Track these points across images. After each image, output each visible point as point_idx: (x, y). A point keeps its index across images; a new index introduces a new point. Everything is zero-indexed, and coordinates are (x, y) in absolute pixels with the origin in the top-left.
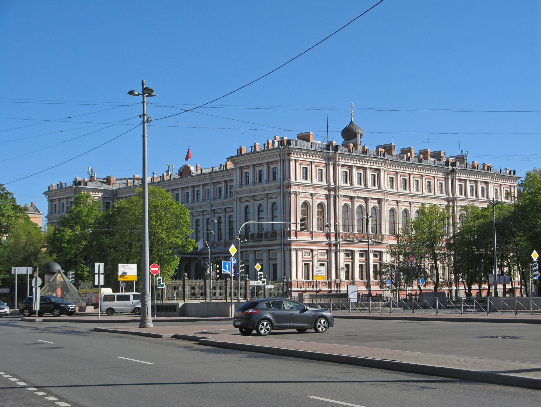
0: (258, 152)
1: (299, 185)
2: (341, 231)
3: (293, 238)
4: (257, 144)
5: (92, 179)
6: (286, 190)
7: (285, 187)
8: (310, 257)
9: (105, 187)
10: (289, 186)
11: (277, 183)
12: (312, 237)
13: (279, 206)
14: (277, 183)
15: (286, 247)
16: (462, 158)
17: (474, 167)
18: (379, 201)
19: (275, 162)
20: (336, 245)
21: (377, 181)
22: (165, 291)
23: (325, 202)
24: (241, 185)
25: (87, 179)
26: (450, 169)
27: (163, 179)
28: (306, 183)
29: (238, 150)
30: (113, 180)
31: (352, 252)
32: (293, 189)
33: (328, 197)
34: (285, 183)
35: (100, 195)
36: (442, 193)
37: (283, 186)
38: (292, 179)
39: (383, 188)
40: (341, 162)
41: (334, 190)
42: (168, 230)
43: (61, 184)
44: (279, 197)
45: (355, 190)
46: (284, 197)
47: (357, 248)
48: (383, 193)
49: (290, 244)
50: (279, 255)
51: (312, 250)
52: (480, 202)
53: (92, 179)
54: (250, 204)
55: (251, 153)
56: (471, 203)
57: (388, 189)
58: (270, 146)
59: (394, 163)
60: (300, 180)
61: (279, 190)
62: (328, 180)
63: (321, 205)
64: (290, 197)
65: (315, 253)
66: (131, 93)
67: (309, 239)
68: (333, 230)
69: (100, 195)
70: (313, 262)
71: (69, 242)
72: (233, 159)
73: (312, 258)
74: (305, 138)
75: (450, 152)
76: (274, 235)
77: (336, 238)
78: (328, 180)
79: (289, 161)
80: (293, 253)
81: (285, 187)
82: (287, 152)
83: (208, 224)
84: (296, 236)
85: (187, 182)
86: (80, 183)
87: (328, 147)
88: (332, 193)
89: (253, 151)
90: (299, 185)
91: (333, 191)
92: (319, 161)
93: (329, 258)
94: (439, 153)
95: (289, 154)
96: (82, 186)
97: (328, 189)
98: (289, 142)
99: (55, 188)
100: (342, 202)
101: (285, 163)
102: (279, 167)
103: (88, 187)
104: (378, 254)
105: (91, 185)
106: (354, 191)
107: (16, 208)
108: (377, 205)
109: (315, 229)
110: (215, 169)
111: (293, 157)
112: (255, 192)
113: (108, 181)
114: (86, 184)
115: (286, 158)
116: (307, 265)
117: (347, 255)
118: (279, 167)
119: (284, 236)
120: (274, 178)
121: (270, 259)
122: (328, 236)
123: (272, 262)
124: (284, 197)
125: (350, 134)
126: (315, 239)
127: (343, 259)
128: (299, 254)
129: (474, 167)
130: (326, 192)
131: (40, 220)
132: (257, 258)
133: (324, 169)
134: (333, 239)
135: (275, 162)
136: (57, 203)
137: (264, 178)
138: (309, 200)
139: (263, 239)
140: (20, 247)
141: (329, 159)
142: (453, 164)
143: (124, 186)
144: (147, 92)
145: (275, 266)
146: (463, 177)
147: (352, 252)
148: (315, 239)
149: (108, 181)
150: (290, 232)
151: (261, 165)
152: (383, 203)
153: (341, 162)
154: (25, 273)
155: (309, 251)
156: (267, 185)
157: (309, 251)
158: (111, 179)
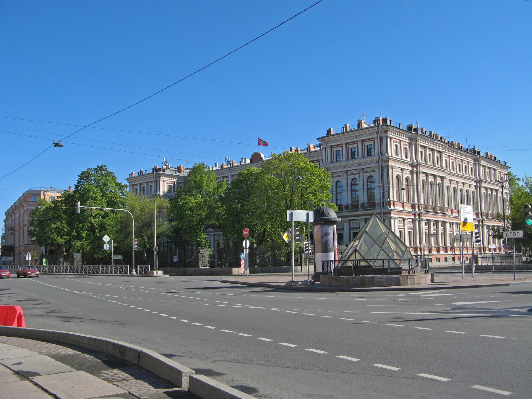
0: (349, 132)
3: (392, 207)
4: (348, 125)
6: (384, 164)
7: (383, 161)
8: (402, 225)
12: (403, 207)
15: (385, 215)
20: (419, 215)
23: (410, 176)
27: (233, 165)
29: (343, 128)
30: (183, 169)
32: (391, 163)
33: (412, 172)
34: (384, 157)
35: (175, 180)
37: (381, 161)
43: (141, 172)
44: (377, 170)
46: (382, 170)
51: (404, 219)
53: (168, 168)
61: (377, 164)
62: (411, 158)
63: (407, 179)
64: (388, 170)
65: (406, 222)
67: (402, 209)
69: (175, 180)
70: (404, 229)
71: (192, 210)
72: (324, 139)
73: (404, 226)
76: (372, 204)
77: (419, 208)
78: (411, 158)
79: (387, 137)
81: (383, 161)
82: (385, 130)
84: (394, 206)
86: (159, 169)
90: (395, 160)
93: (414, 226)
95: (160, 177)
96: (161, 172)
101: (382, 140)
103: (165, 173)
105: (167, 172)
109: (405, 201)
111: (162, 179)
112: (349, 167)
114: (164, 171)
115: (383, 135)
119: (383, 206)
121: (350, 228)
122: (413, 207)
124: (382, 170)
127: (424, 227)
132: (351, 227)
139: (359, 210)
149: (179, 169)
150: (389, 202)
153: (421, 142)
154: (304, 220)
155: (402, 219)
156: (363, 160)
157: (402, 219)
158: (182, 168)
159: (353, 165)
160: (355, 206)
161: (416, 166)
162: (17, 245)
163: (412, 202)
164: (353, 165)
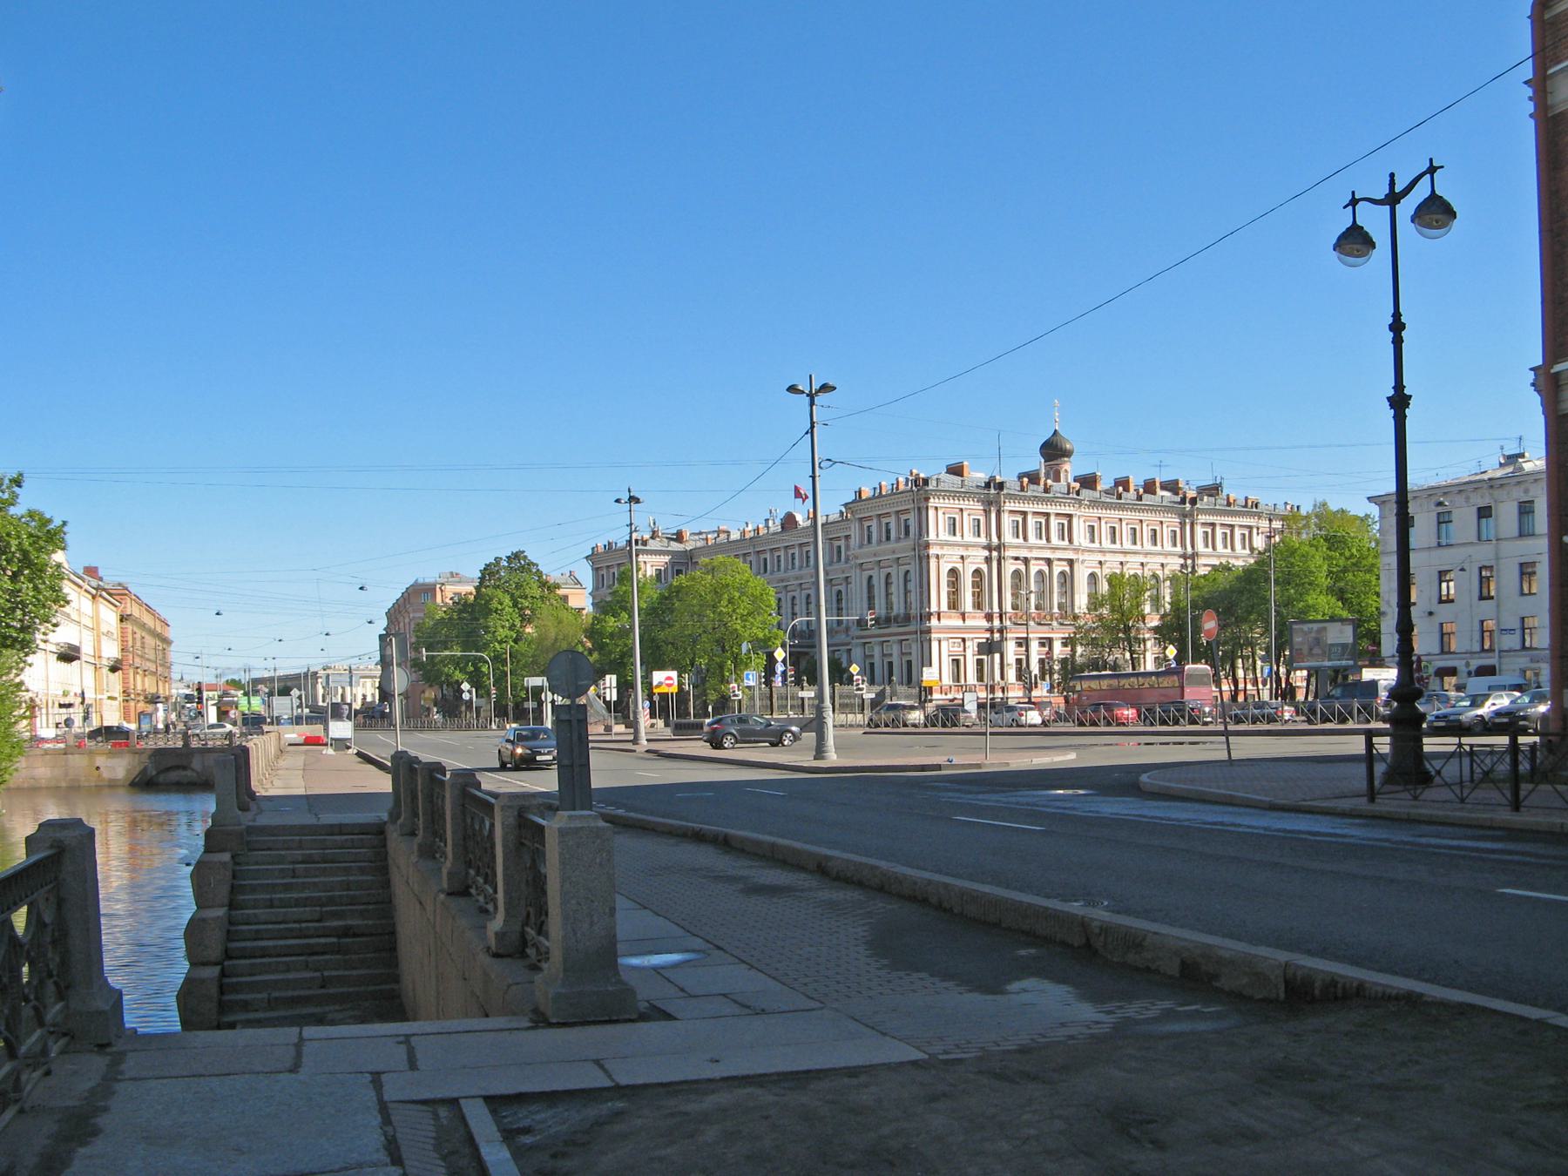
1: (942, 545)
2: (1009, 609)
3: (934, 622)
5: (654, 535)
9: (675, 546)
10: (927, 546)
11: (909, 543)
13: (913, 576)
14: (909, 543)
16: (1213, 490)
17: (1229, 504)
18: (1071, 562)
19: (907, 511)
20: (1001, 631)
21: (1067, 532)
22: (744, 703)
23: (984, 567)
24: (861, 546)
25: (647, 536)
26: (1186, 505)
28: (953, 542)
30: (687, 536)
31: (1050, 640)
32: (933, 551)
33: (988, 560)
35: (667, 559)
36: (1175, 545)
38: (932, 536)
39: (1076, 542)
40: (1009, 506)
41: (999, 548)
42: (743, 618)
45: (1030, 548)
47: (1036, 634)
48: (1076, 550)
49: (929, 631)
50: (915, 648)
51: (964, 640)
52: (1237, 558)
54: (893, 570)
55: (893, 494)
56: (1224, 561)
57: (1086, 543)
58: (902, 487)
59: (1094, 504)
60: (945, 536)
62: (988, 535)
63: (977, 572)
66: (618, 501)
67: (959, 623)
68: (996, 609)
69: (667, 559)
71: (612, 636)
74: (956, 470)
75: (1192, 478)
76: (907, 619)
78: (988, 535)
80: (935, 645)
83: (793, 605)
85: (791, 539)
87: (988, 485)
88: (995, 554)
89: (878, 496)
90: (942, 545)
91: (996, 550)
92: (974, 508)
94: (1176, 482)
95: (927, 499)
97: (989, 548)
98: (926, 482)
99: (601, 550)
100: (1010, 567)
101: (922, 512)
102: (912, 518)
104: (1047, 642)
105: (653, 545)
106: (1028, 548)
107: (543, 584)
108: (1067, 569)
110: (831, 519)
111: (933, 502)
113: (679, 537)
114: (645, 543)
115: (923, 505)
116: (956, 662)
117: (1042, 645)
118: (912, 518)
120: (907, 533)
122: (989, 617)
123: (905, 659)
125: (1053, 451)
126: (969, 623)
128: (944, 644)
129: (1229, 504)
130: (986, 553)
131: (581, 600)
133: (982, 519)
134: (996, 623)
135: (907, 511)
136: (604, 572)
137: (893, 535)
138: (959, 566)
140: (548, 643)
141: (990, 503)
142: (1193, 501)
143: (700, 544)
144: (633, 500)
145: (890, 664)
146: (1210, 519)
147: (1050, 640)
148: (969, 623)
149: (679, 537)
151: (888, 514)
152: (1076, 566)
153: (1009, 506)
159: (886, 551)
160: (888, 620)
161: (999, 548)
162: (414, 858)
163: (987, 610)
164: (886, 551)
